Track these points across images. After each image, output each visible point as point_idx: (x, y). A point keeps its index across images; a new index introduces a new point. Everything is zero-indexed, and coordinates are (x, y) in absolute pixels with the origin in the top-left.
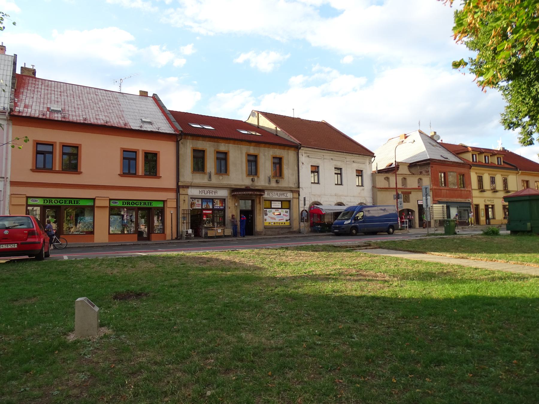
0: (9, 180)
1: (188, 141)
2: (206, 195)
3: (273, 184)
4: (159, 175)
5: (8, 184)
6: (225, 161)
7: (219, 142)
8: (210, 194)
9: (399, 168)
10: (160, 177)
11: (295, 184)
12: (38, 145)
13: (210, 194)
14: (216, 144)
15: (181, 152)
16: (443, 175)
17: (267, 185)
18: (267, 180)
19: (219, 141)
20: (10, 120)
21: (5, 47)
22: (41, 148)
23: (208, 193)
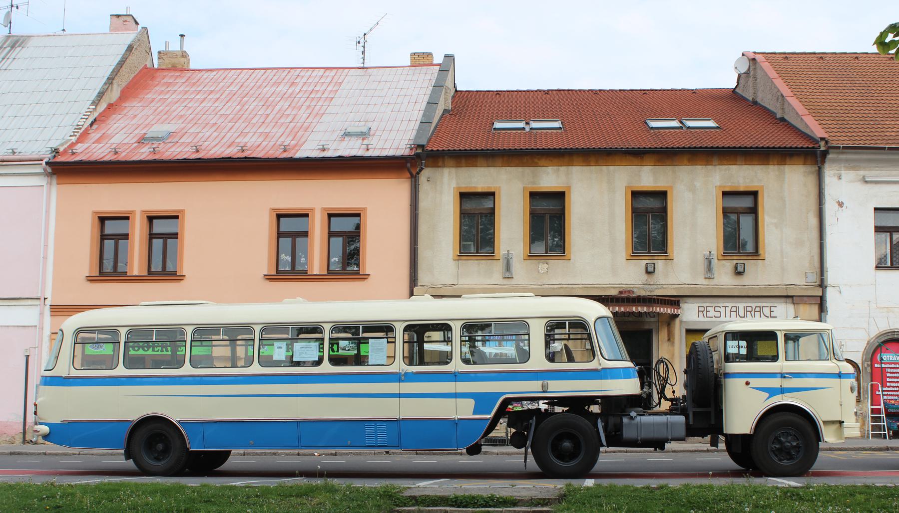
0: (48, 302)
1: (446, 171)
3: (724, 278)
4: (364, 269)
5: (47, 310)
7: (536, 165)
10: (365, 277)
11: (809, 275)
12: (332, 218)
14: (528, 170)
15: (423, 204)
17: (701, 281)
18: (701, 267)
19: (536, 160)
20: (54, 174)
22: (288, 225)
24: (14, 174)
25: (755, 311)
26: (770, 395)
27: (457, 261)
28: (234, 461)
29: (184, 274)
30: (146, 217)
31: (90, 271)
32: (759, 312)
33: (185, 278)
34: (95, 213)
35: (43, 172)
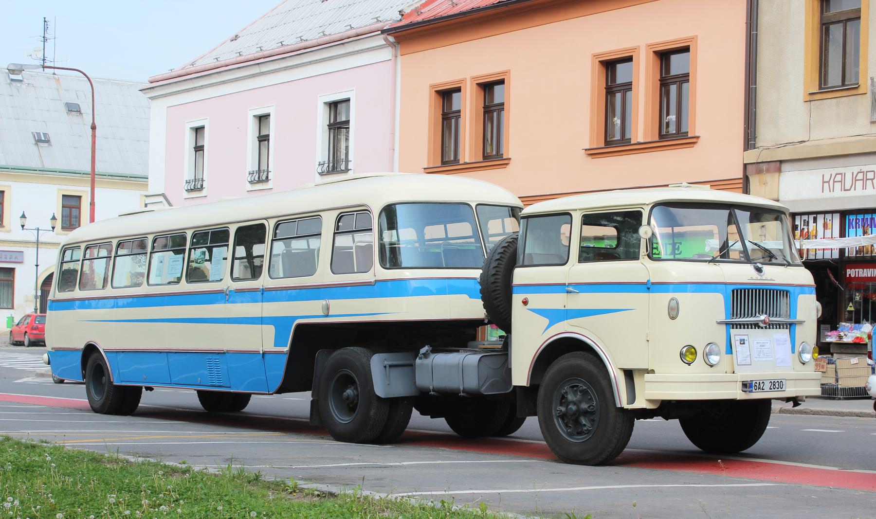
2: (847, 194)
6: (339, 106)
8: (864, 187)
9: (852, 388)
13: (864, 187)
16: (426, 243)
21: (79, 226)
23: (859, 184)
24: (310, 63)
25: (834, 182)
26: (550, 322)
27: (809, 103)
28: (65, 381)
29: (510, 157)
30: (652, 53)
31: (591, 144)
32: (862, 181)
33: (700, 141)
34: (432, 86)
35: (385, 43)
